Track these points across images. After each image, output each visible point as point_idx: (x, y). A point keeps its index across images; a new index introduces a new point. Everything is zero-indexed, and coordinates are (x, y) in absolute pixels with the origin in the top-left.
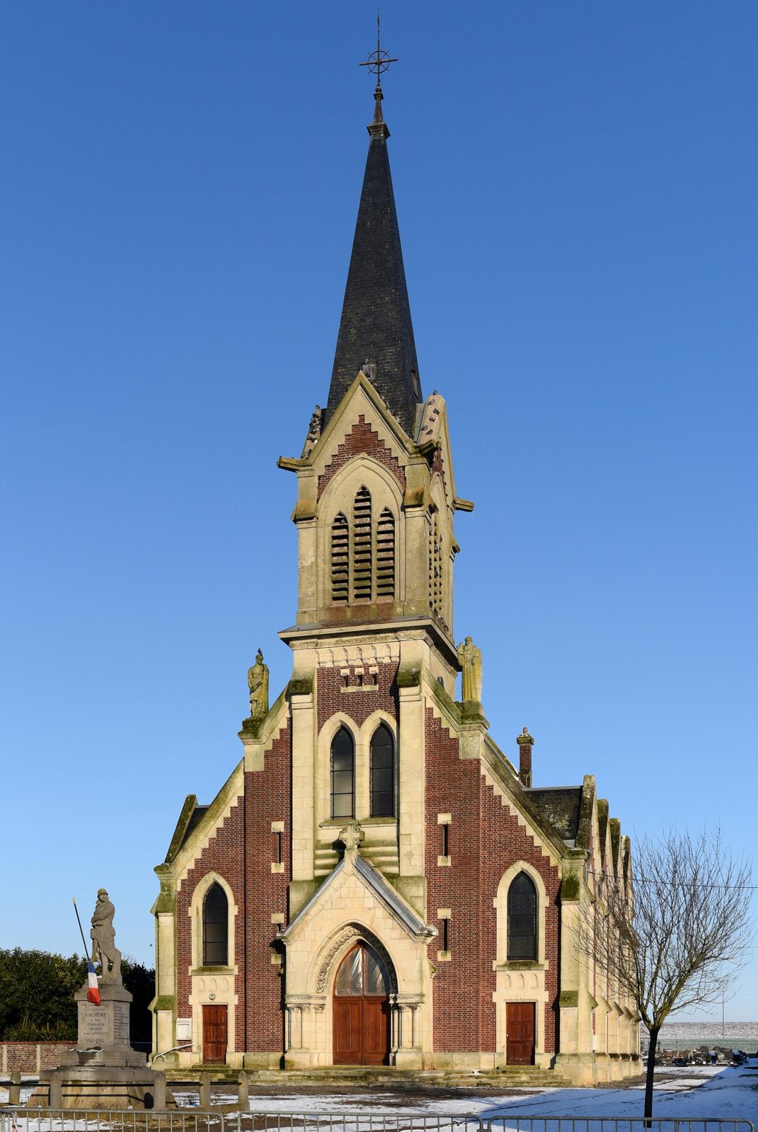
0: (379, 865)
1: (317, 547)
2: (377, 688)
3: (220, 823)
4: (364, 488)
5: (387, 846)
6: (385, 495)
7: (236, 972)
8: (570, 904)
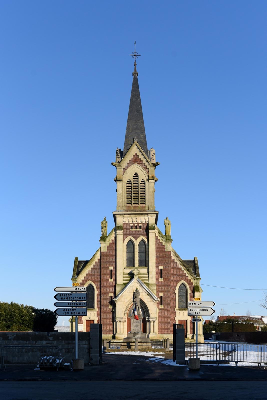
0: (143, 280)
1: (123, 188)
2: (141, 230)
3: (92, 266)
4: (136, 173)
5: (145, 275)
6: (143, 176)
7: (97, 310)
8: (197, 293)
